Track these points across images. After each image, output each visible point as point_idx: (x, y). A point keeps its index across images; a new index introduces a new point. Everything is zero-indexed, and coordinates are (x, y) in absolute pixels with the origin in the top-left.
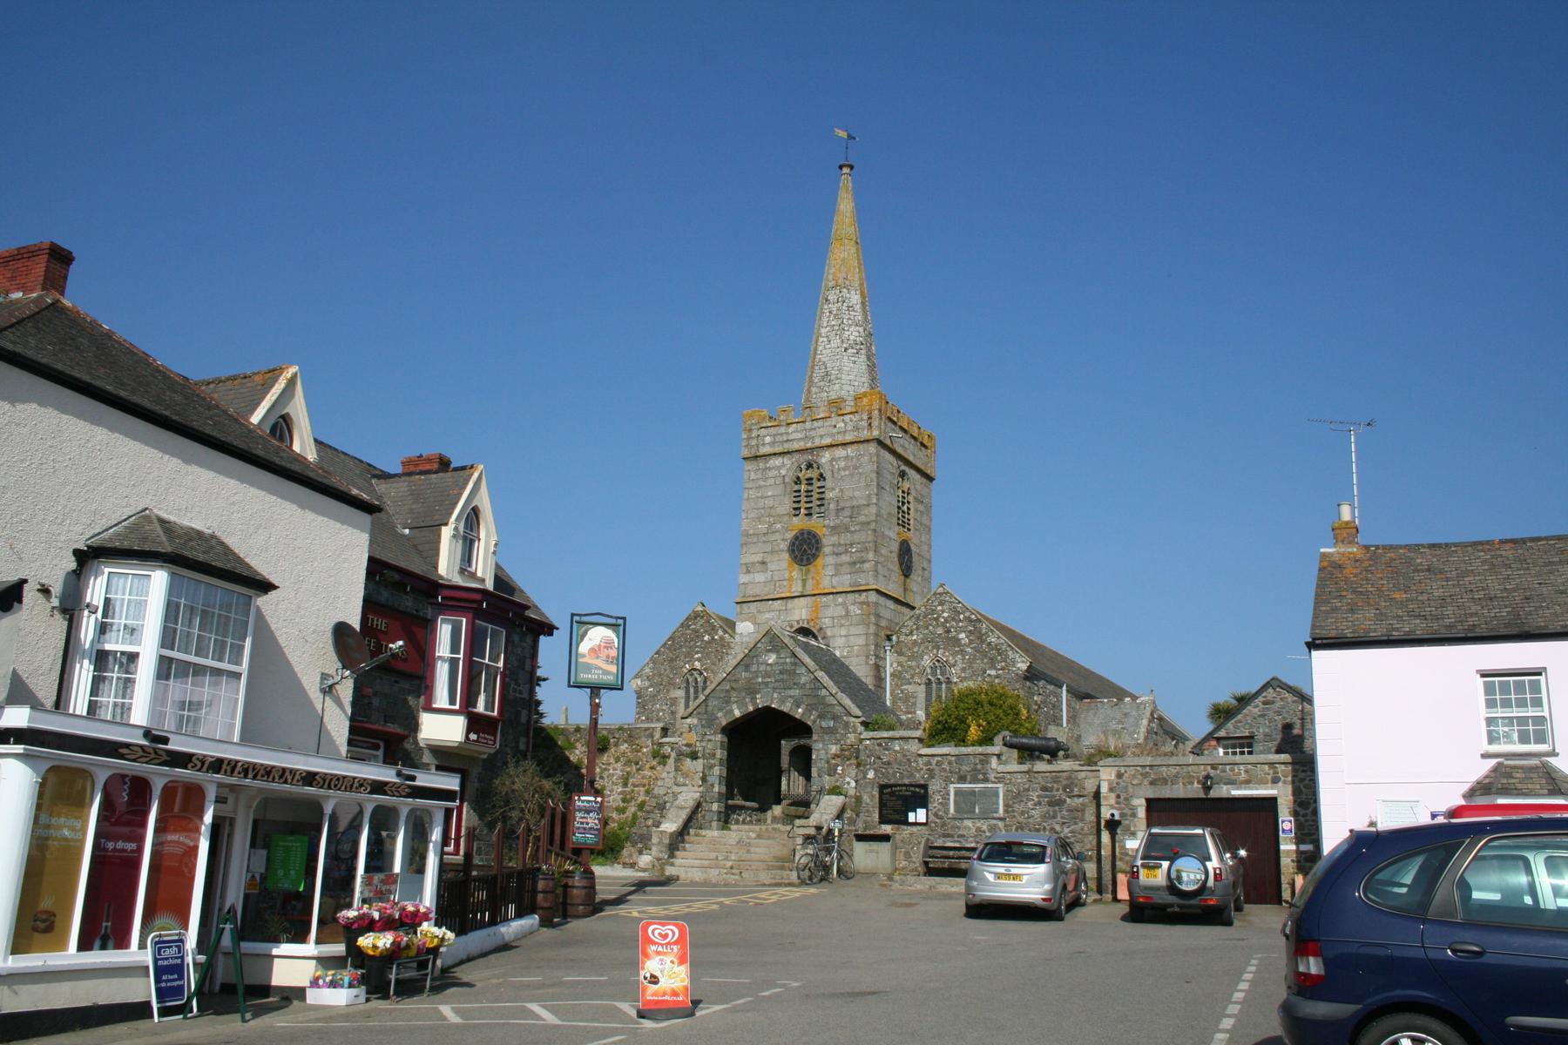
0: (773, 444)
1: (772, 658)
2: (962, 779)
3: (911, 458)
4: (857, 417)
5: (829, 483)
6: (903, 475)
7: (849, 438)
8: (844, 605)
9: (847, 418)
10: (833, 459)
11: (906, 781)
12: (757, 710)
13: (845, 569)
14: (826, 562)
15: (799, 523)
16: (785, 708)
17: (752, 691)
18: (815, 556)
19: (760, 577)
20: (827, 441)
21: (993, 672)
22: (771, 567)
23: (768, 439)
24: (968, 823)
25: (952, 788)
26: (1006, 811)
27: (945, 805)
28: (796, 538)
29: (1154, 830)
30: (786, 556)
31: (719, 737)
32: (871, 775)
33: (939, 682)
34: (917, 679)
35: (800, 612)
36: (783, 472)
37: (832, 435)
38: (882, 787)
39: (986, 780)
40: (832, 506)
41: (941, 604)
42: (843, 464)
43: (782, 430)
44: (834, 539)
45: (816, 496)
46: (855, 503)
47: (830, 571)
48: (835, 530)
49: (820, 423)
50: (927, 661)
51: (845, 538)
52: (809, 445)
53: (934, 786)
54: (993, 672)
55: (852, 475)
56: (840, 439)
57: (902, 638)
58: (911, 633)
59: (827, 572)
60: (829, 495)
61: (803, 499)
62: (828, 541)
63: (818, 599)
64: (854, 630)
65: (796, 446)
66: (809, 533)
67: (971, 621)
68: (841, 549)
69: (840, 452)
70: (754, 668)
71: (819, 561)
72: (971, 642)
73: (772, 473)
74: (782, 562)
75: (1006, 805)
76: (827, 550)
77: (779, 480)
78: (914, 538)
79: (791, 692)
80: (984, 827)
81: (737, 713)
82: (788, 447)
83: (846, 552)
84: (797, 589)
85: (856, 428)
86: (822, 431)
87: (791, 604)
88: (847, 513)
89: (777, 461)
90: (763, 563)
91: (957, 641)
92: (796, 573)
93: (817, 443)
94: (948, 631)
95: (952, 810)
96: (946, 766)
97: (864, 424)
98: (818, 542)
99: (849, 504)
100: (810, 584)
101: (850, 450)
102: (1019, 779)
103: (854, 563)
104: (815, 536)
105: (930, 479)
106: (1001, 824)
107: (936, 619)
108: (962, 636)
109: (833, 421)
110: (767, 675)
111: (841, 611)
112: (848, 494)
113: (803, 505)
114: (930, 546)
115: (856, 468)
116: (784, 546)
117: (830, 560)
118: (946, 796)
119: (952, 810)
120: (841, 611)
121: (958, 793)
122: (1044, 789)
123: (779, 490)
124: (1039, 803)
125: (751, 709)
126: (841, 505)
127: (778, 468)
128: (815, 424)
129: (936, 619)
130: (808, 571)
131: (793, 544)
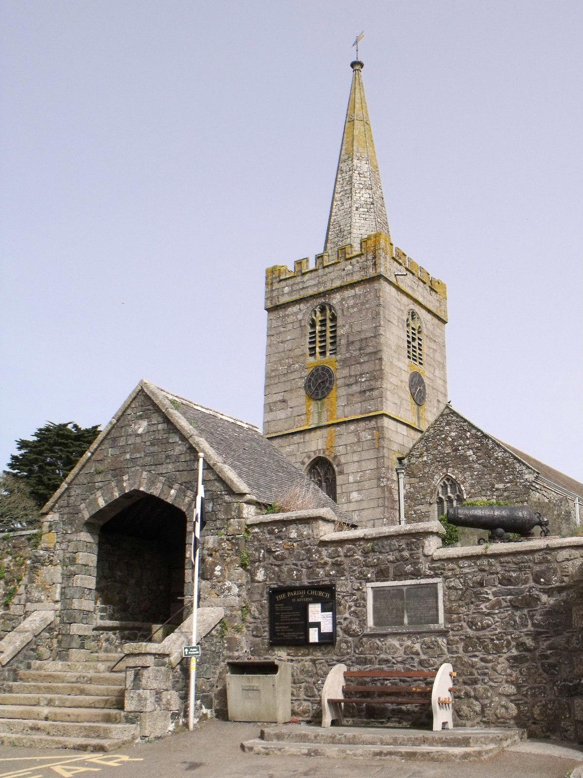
0: (290, 293)
1: (142, 427)
2: (382, 575)
3: (420, 299)
4: (363, 258)
5: (340, 322)
6: (413, 314)
7: (356, 278)
8: (356, 433)
9: (354, 261)
10: (343, 299)
11: (306, 582)
12: (125, 496)
13: (356, 399)
14: (339, 396)
15: (318, 360)
16: (156, 492)
17: (118, 472)
18: (329, 389)
19: (281, 415)
20: (337, 283)
21: (501, 486)
22: (291, 404)
23: (286, 290)
24: (394, 642)
25: (369, 590)
26: (448, 620)
27: (361, 617)
28: (312, 374)
29: (343, 704)
30: (303, 392)
31: (85, 537)
32: (260, 575)
33: (450, 500)
34: (428, 499)
35: (316, 444)
36: (300, 317)
37: (341, 277)
38: (274, 593)
39: (416, 574)
40: (343, 342)
41: (448, 424)
42: (351, 302)
43: (299, 279)
44: (345, 372)
45: (329, 335)
46: (363, 336)
47: (342, 402)
48: (345, 363)
49: (331, 269)
50: (437, 481)
51: (356, 370)
52: (322, 289)
53: (343, 586)
54: (501, 486)
55: (360, 311)
56: (349, 280)
57: (413, 460)
58: (421, 455)
59: (341, 404)
60: (340, 332)
61: (318, 339)
62: (340, 374)
63: (333, 429)
64: (366, 455)
65: (311, 292)
66: (323, 368)
67: (477, 437)
68: (352, 380)
69: (350, 293)
70: (122, 442)
71: (333, 394)
72: (479, 458)
73: (290, 320)
74: (299, 399)
75: (448, 611)
76: (339, 382)
77: (297, 325)
78: (426, 373)
79: (163, 469)
80: (417, 647)
81: (102, 503)
82: (304, 294)
83: (356, 382)
84: (313, 423)
85: (363, 268)
86: (332, 276)
87: (308, 436)
88: (357, 345)
89: (295, 309)
90: (284, 401)
91: (465, 459)
92: (313, 406)
93: (328, 288)
94: (457, 450)
95: (370, 622)
96: (358, 556)
97: (370, 263)
98: (331, 376)
99: (358, 338)
100: (325, 415)
101: (358, 290)
102: (467, 568)
103: (364, 391)
104: (328, 370)
105: (445, 322)
106: (442, 641)
107: (445, 439)
108: (470, 452)
109: (343, 264)
110: (136, 449)
111: (353, 439)
112: (356, 328)
113: (318, 344)
114: (445, 381)
115: (363, 304)
116: (301, 383)
117: (343, 391)
118: (361, 602)
119: (370, 622)
120: (353, 439)
121: (377, 592)
122: (506, 581)
123: (296, 333)
124: (498, 604)
125: (117, 495)
126: (351, 339)
127: (296, 314)
128: (327, 270)
129: (445, 439)
130: (322, 404)
131: (309, 380)
